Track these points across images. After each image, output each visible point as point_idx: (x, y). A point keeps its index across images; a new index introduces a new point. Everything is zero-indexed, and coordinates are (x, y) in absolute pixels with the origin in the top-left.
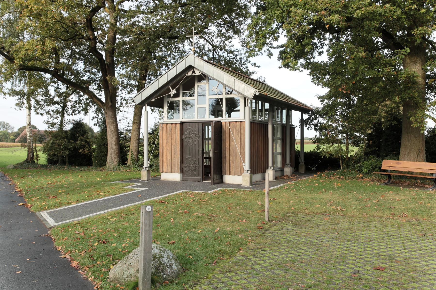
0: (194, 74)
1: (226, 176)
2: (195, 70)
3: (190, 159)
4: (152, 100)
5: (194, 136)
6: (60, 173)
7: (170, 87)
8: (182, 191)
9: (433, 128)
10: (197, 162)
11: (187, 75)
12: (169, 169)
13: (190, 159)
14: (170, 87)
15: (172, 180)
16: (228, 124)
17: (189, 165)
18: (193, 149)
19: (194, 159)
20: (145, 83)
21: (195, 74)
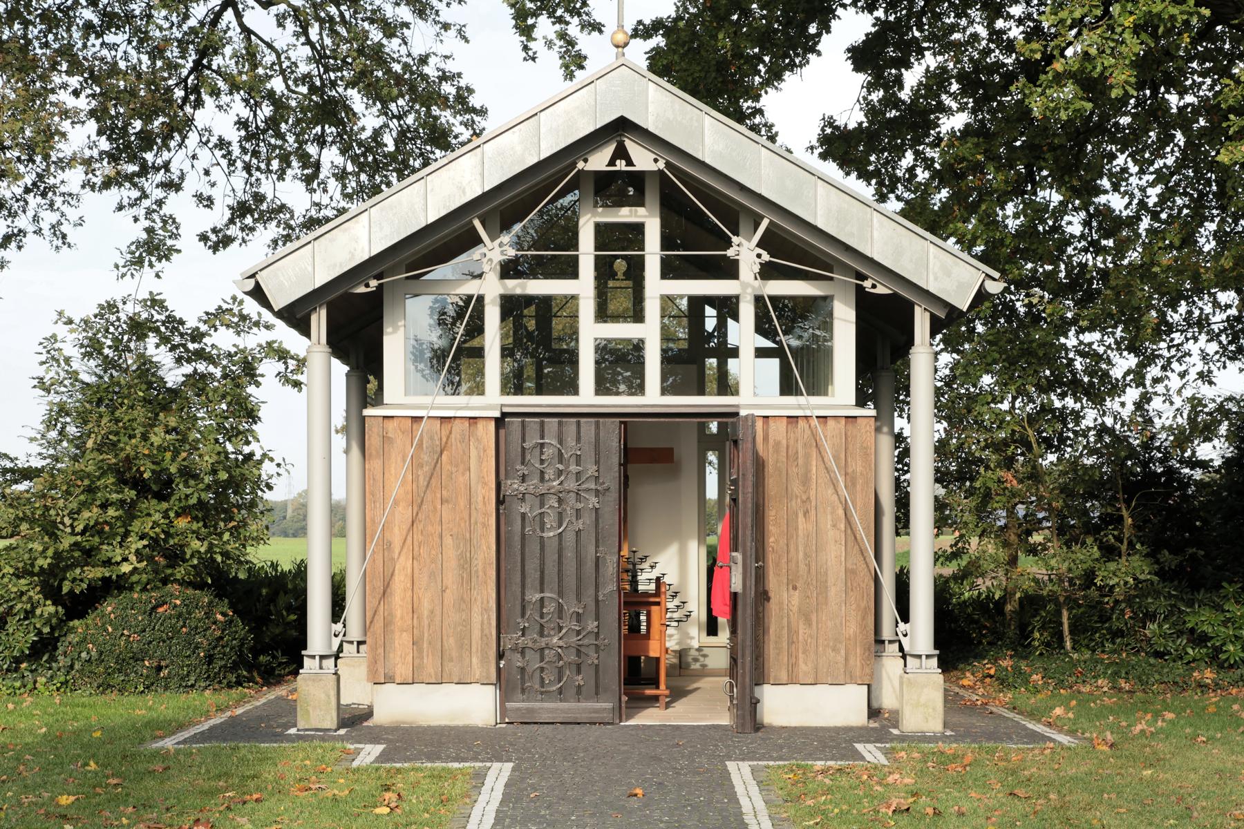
0: (621, 165)
1: (766, 686)
2: (632, 147)
3: (550, 608)
4: (362, 289)
5: (571, 485)
6: (1090, 672)
7: (477, 223)
8: (1030, 726)
9: (674, 15)
10: (592, 625)
11: (581, 165)
12: (430, 665)
13: (550, 608)
14: (477, 223)
15: (444, 723)
16: (778, 431)
17: (543, 642)
18: (570, 554)
19: (572, 607)
20: (1230, 445)
21: (630, 163)
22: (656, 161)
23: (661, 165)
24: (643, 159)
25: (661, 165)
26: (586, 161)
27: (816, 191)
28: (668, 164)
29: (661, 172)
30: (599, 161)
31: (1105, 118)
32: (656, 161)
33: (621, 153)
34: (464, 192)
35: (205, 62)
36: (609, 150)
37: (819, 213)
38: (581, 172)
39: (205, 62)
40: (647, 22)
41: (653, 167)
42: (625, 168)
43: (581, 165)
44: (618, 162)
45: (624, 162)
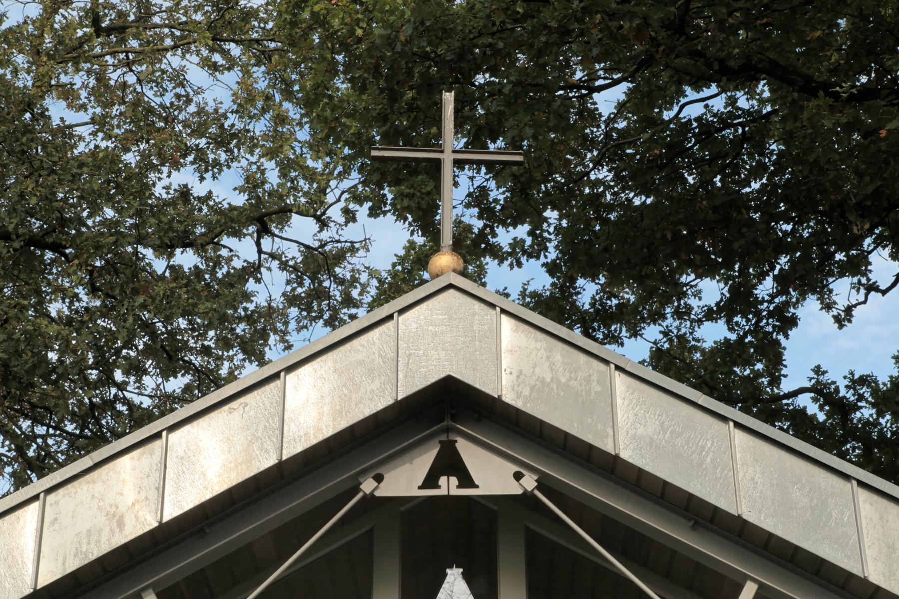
0: (449, 486)
2: (472, 455)
21: (466, 481)
22: (518, 476)
23: (529, 482)
24: (493, 474)
25: (529, 482)
26: (379, 479)
27: (731, 446)
28: (542, 485)
29: (526, 498)
30: (404, 478)
31: (844, 320)
32: (518, 476)
33: (450, 464)
34: (121, 524)
35: (284, 259)
36: (424, 461)
37: (870, 553)
38: (371, 501)
39: (284, 259)
40: (402, 253)
41: (515, 489)
42: (455, 491)
43: (368, 486)
44: (443, 480)
45: (454, 481)
